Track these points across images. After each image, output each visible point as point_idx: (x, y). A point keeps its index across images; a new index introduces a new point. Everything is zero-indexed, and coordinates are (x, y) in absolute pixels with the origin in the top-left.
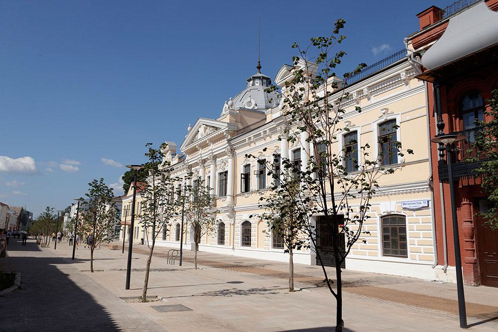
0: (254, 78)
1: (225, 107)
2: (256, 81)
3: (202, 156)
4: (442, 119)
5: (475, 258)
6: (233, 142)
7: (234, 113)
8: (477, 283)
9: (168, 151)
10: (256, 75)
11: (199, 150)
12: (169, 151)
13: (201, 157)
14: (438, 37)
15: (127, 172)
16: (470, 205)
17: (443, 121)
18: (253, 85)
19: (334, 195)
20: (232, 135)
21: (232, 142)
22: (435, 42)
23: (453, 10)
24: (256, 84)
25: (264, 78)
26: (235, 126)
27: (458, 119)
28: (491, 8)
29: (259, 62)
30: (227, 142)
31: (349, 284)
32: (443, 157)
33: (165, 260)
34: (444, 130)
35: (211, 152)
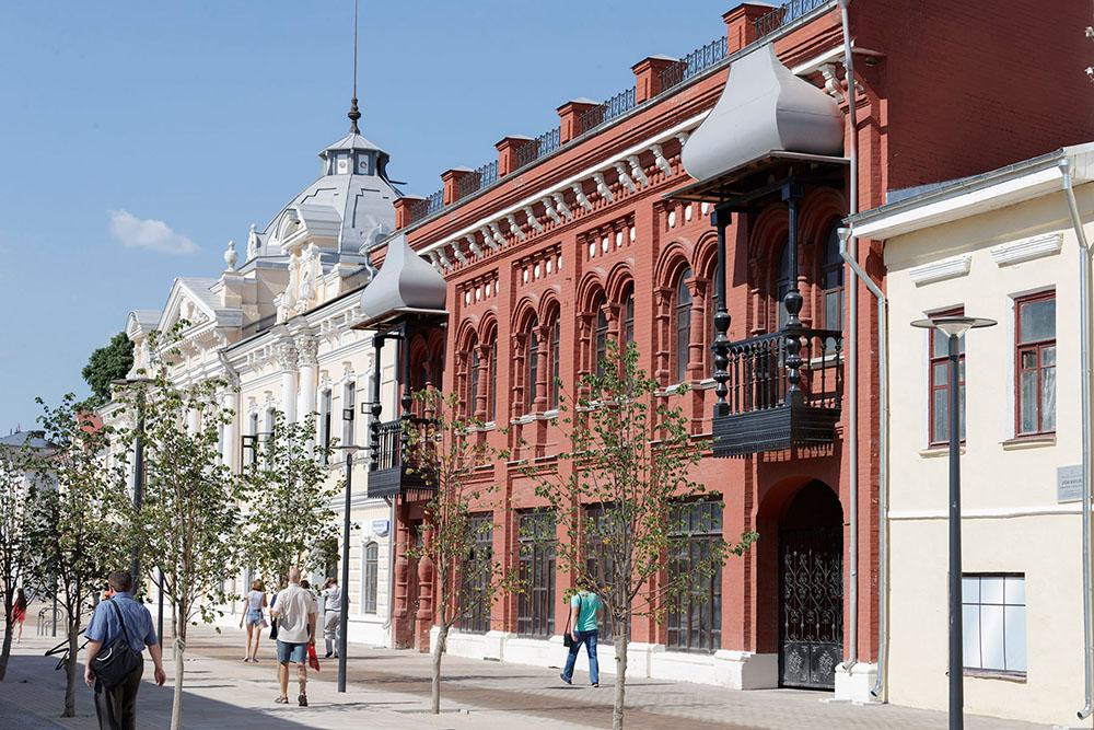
0: (334, 153)
1: (250, 240)
2: (339, 161)
3: (207, 368)
4: (724, 305)
5: (405, 609)
6: (233, 356)
7: (236, 281)
8: (402, 645)
9: (306, 243)
10: (336, 146)
11: (199, 353)
12: (311, 245)
13: (206, 373)
14: (710, 101)
15: (100, 352)
16: (406, 531)
17: (726, 311)
18: (330, 173)
19: (352, 499)
20: (232, 337)
21: (229, 355)
22: (707, 112)
23: (515, 156)
24: (340, 171)
25: (358, 151)
26: (236, 316)
27: (814, 285)
28: (781, 60)
29: (355, 102)
30: (217, 355)
31: (627, 708)
32: (724, 399)
33: (298, 693)
34: (728, 332)
35: (201, 370)
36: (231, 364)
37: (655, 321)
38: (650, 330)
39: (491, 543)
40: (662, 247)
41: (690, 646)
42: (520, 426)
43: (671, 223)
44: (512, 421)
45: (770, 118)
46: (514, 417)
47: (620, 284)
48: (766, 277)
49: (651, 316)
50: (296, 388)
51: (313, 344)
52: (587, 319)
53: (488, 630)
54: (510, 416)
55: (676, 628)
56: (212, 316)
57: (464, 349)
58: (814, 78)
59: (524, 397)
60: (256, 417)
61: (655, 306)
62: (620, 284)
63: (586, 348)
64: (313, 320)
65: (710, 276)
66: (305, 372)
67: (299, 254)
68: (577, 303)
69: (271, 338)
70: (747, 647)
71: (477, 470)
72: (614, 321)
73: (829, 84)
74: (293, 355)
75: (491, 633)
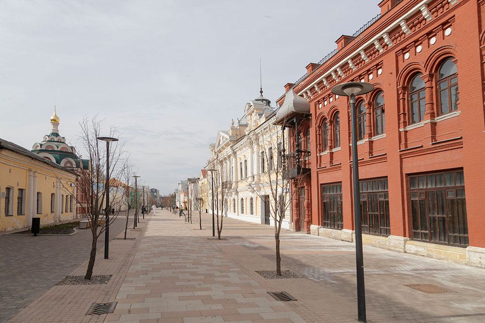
6: (234, 147)
12: (255, 111)
36: (234, 150)
37: (316, 135)
38: (480, 69)
39: (342, 194)
40: (400, 70)
41: (422, 238)
42: (321, 156)
43: (320, 107)
44: (402, 130)
45: (292, 105)
46: (402, 125)
47: (333, 113)
48: (405, 94)
49: (480, 62)
50: (253, 153)
51: (257, 139)
52: (404, 88)
53: (342, 228)
54: (349, 143)
55: (462, 235)
56: (228, 138)
57: (320, 124)
58: (302, 96)
59: (322, 146)
60: (241, 163)
61: (316, 131)
62: (333, 113)
63: (319, 136)
64: (257, 131)
65: (333, 119)
66: (255, 147)
67: (251, 115)
68: (397, 83)
69: (245, 139)
70: (405, 236)
71: (370, 158)
72: (430, 82)
73: (305, 97)
74: (251, 143)
75: (344, 230)
